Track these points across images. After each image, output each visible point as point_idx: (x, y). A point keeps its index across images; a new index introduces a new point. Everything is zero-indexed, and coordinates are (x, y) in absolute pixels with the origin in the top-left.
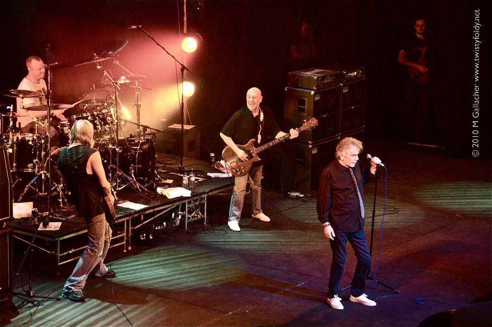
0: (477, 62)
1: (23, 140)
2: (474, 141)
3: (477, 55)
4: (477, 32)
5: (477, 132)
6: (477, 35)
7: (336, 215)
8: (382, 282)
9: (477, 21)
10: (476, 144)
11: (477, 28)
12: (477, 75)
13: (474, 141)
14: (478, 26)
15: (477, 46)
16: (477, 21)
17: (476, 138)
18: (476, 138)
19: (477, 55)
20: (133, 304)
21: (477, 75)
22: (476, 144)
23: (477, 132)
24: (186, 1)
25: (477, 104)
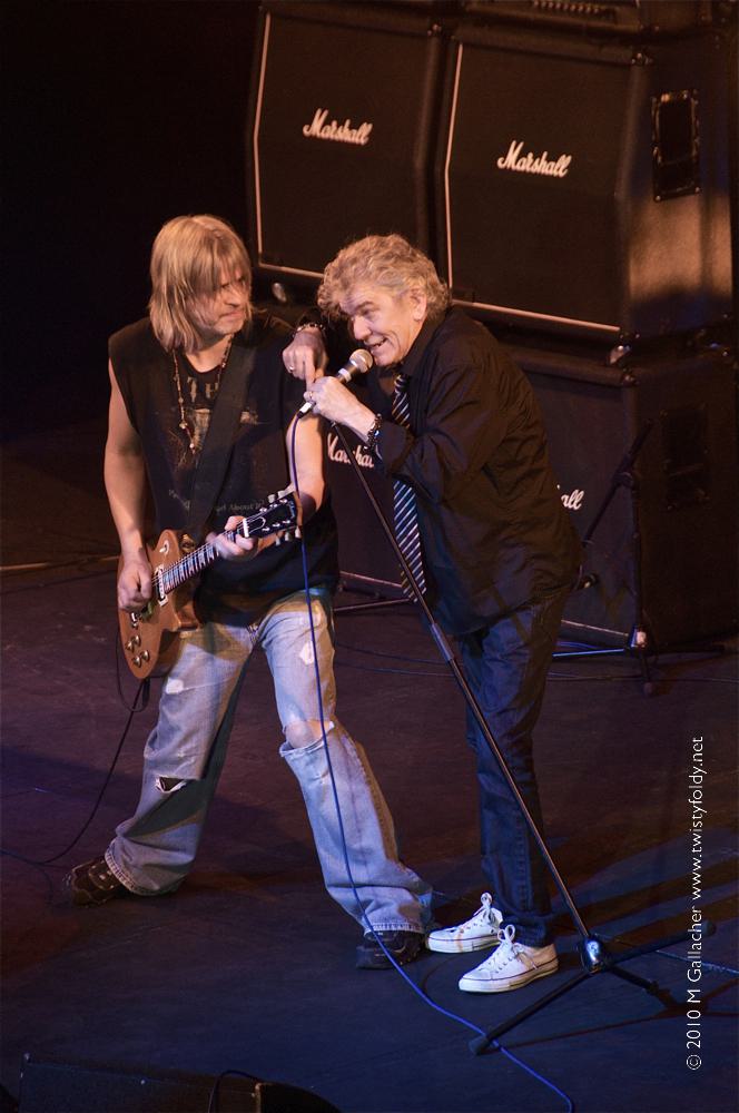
0: (697, 855)
1: (180, 591)
2: (691, 1034)
3: (697, 840)
4: (697, 789)
5: (696, 1014)
6: (698, 795)
7: (443, 420)
8: (625, 982)
9: (697, 764)
10: (696, 1041)
11: (698, 779)
12: (698, 872)
13: (691, 1034)
14: (700, 773)
15: (696, 821)
16: (697, 764)
17: (693, 1021)
18: (693, 1021)
19: (697, 840)
20: (227, 224)
21: (698, 872)
22: (696, 1041)
23: (696, 1014)
24: (2, 566)
25: (696, 950)
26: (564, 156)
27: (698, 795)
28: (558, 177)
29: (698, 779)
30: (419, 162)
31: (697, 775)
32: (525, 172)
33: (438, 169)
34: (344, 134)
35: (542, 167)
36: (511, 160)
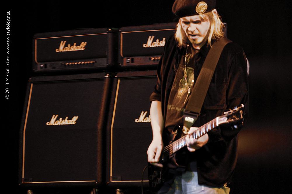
0: (8, 42)
3: (8, 38)
4: (8, 25)
6: (8, 27)
9: (8, 19)
10: (8, 91)
11: (8, 23)
14: (9, 21)
15: (8, 33)
16: (8, 19)
17: (8, 88)
18: (8, 88)
19: (8, 38)
22: (8, 91)
26: (236, 107)
27: (8, 27)
28: (73, 124)
29: (8, 23)
30: (99, 126)
31: (8, 21)
32: (59, 125)
33: (108, 127)
34: (66, 122)
35: (66, 122)
36: (53, 122)
